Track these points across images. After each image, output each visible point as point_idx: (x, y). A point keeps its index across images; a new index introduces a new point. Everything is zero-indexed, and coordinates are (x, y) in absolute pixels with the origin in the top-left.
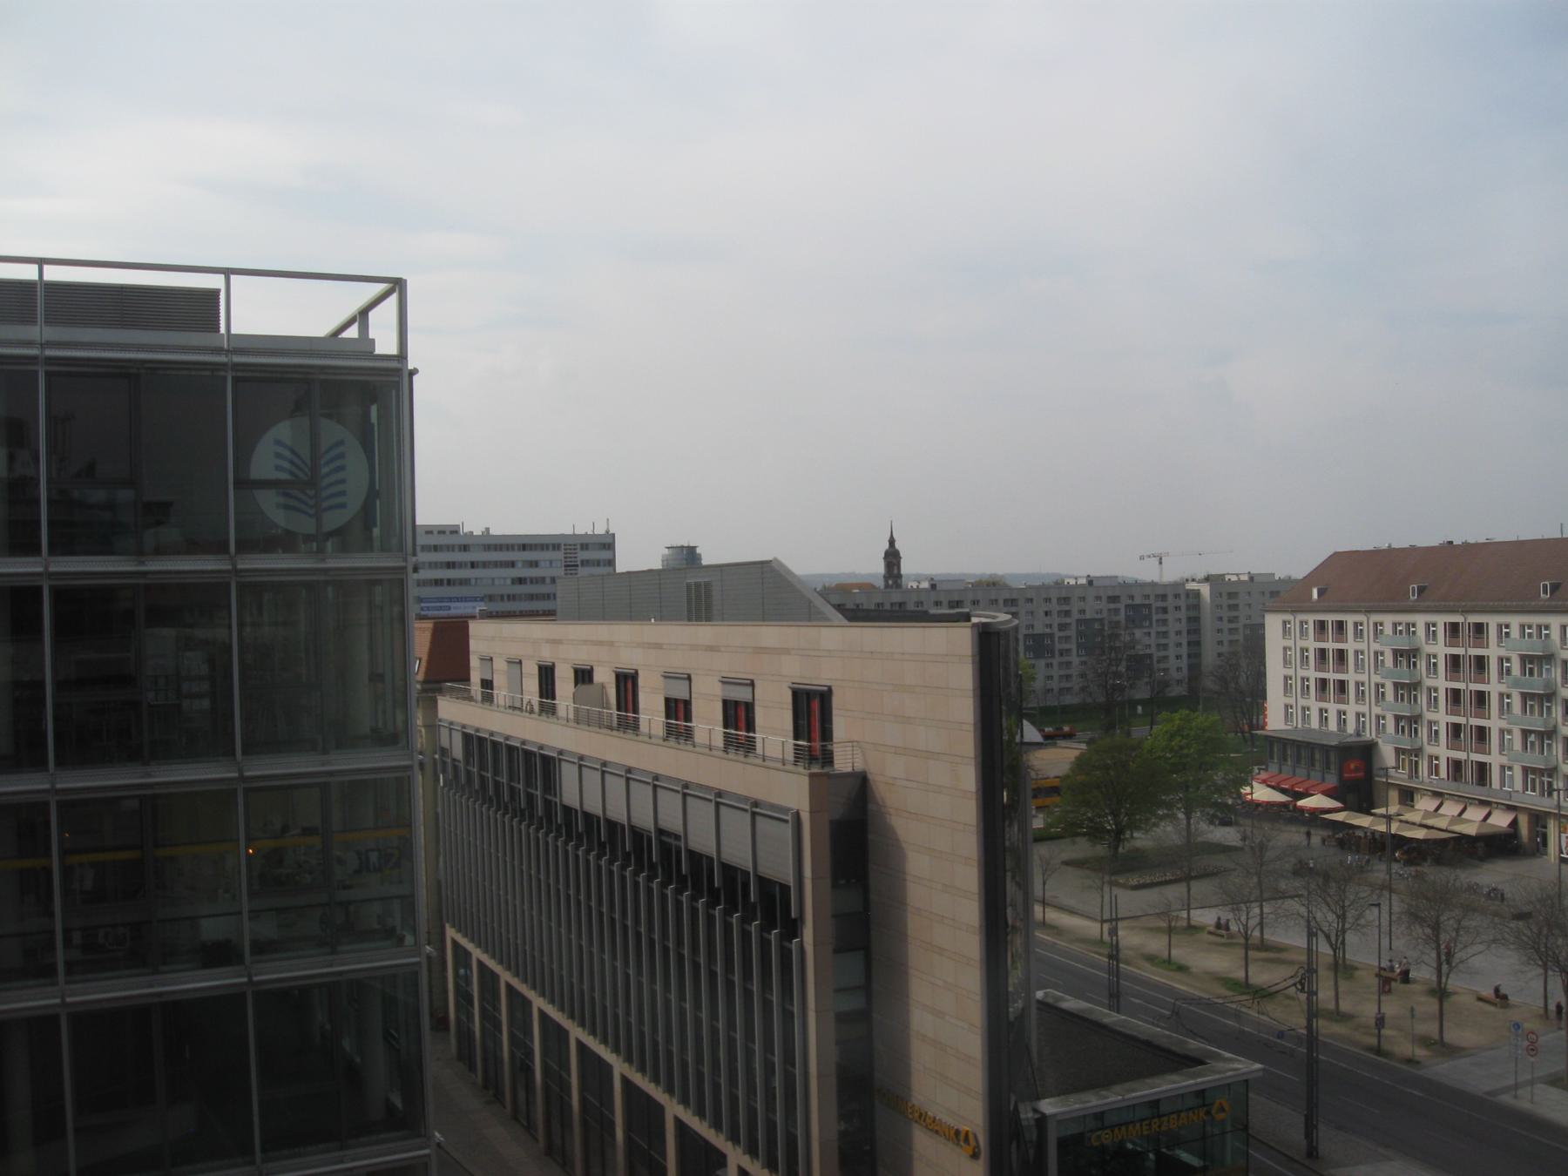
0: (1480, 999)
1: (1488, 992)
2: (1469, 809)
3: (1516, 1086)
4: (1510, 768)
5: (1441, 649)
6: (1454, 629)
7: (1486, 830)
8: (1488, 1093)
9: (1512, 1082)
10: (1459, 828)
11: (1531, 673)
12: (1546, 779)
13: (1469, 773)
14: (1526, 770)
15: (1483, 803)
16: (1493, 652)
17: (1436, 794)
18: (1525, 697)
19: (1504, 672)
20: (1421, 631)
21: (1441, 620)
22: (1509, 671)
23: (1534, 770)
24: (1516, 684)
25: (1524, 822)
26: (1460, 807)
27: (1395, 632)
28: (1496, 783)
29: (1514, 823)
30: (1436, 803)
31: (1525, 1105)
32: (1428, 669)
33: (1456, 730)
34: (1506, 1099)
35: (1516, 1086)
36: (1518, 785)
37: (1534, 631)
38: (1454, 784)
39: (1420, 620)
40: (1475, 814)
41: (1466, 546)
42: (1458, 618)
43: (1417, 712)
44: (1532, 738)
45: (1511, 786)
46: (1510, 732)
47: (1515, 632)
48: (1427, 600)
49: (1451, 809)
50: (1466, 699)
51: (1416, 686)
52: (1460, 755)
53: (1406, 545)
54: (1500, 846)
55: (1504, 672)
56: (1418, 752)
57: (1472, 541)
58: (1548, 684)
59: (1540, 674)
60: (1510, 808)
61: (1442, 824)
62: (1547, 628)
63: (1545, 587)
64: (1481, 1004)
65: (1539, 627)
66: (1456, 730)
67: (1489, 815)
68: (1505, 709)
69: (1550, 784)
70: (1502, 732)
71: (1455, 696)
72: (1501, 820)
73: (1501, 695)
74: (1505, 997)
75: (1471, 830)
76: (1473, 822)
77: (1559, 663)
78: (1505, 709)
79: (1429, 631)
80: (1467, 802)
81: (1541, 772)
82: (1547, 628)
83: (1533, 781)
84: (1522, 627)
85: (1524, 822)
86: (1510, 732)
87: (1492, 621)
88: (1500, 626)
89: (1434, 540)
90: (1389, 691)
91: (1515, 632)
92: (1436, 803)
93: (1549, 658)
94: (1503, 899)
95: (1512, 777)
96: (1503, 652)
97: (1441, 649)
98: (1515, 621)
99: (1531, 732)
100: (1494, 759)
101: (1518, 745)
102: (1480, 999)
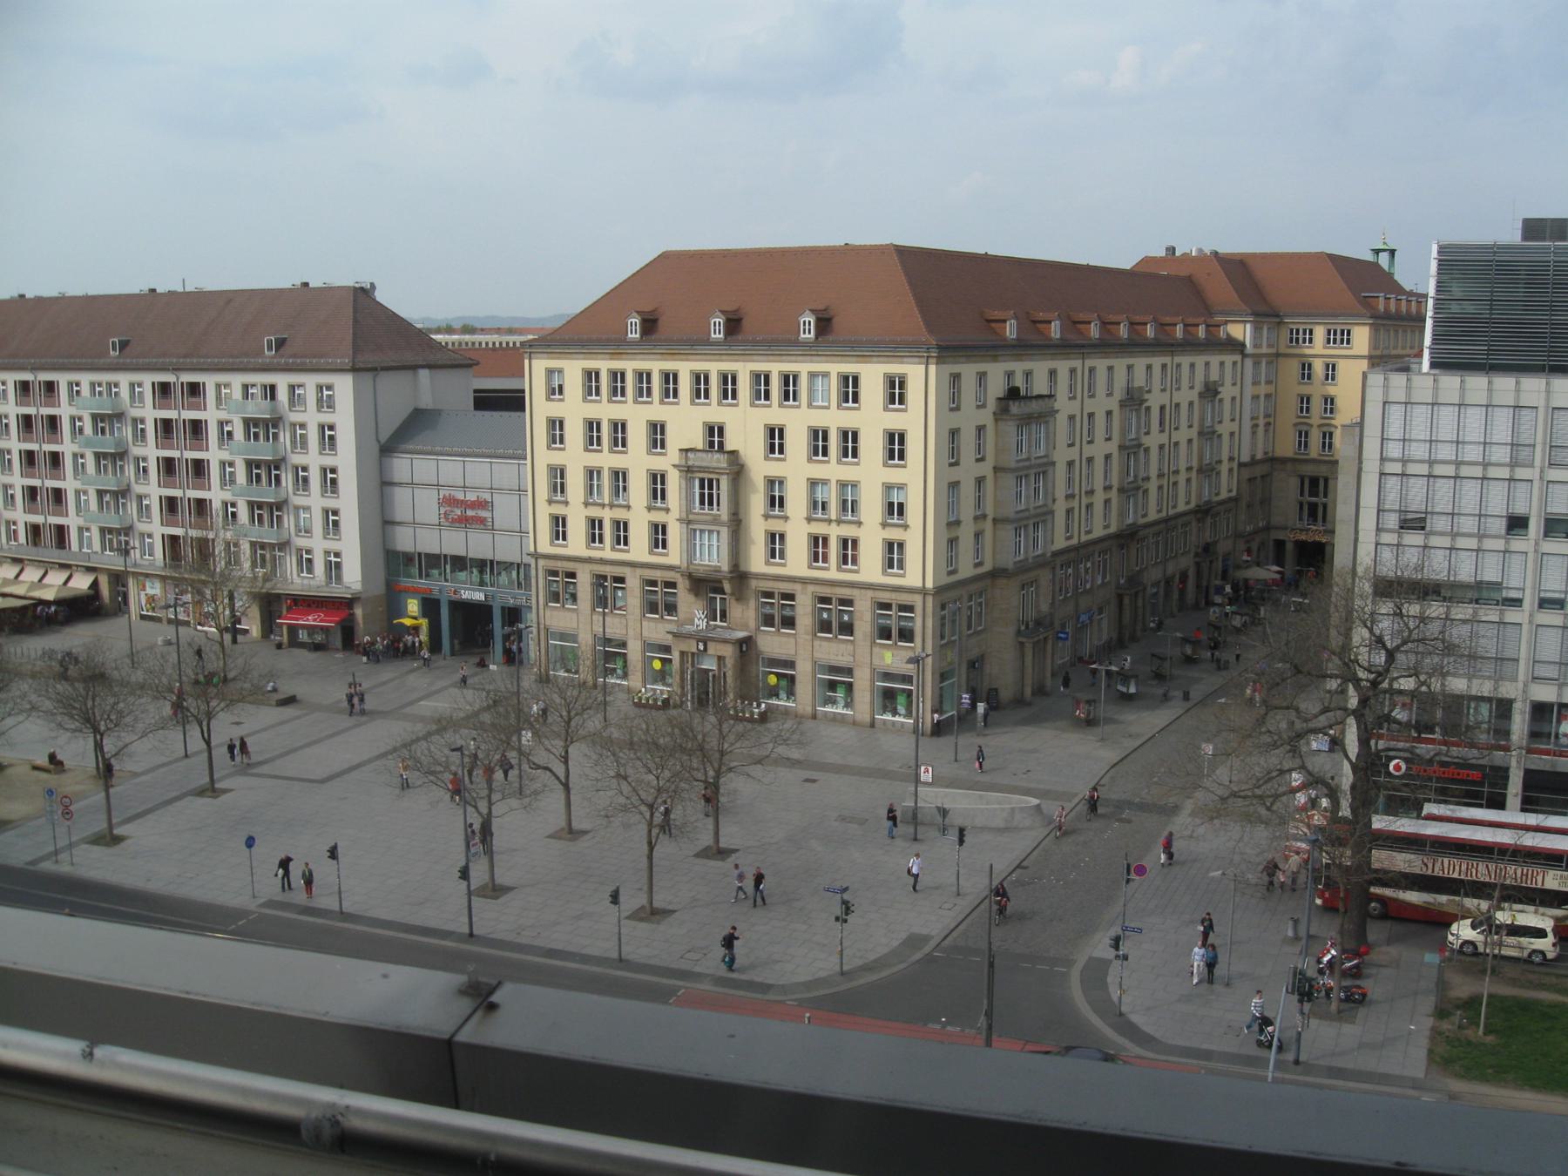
0: (36, 768)
1: (43, 761)
2: (50, 574)
3: (56, 853)
4: (88, 529)
5: (150, 413)
6: (164, 390)
7: (65, 594)
8: (32, 863)
9: (52, 849)
10: (37, 594)
11: (103, 432)
12: (123, 538)
13: (48, 537)
14: (103, 531)
15: (63, 566)
16: (64, 411)
17: (16, 561)
18: (98, 456)
19: (77, 431)
20: (282, 395)
21: (148, 379)
22: (81, 430)
23: (110, 531)
24: (88, 444)
25: (104, 582)
26: (41, 572)
27: (246, 395)
28: (75, 546)
29: (95, 585)
30: (16, 570)
31: (65, 868)
32: (294, 442)
33: (32, 493)
34: (48, 866)
35: (56, 853)
36: (97, 546)
37: (103, 389)
38: (34, 549)
39: (124, 379)
40: (56, 578)
41: (39, 300)
42: (168, 378)
43: (283, 496)
44: (107, 498)
45: (90, 546)
46: (85, 493)
47: (85, 390)
48: (129, 356)
49: (31, 575)
50: (40, 460)
51: (277, 464)
52: (38, 519)
53: (54, 294)
54: (80, 609)
55: (77, 431)
56: (128, 530)
57: (90, 293)
58: (119, 443)
59: (112, 433)
60: (90, 569)
61: (19, 590)
62: (140, 385)
63: (270, 342)
64: (36, 773)
65: (109, 385)
66: (32, 493)
67: (21, 571)
68: (79, 469)
69: (127, 543)
70: (78, 492)
71: (168, 466)
72: (81, 583)
73: (75, 455)
74: (61, 763)
75: (49, 595)
76: (53, 586)
77: (129, 422)
78: (79, 469)
79: (135, 392)
80: (47, 567)
81: (119, 532)
82: (116, 385)
83: (111, 541)
84: (93, 385)
85: (104, 582)
86: (85, 493)
87: (62, 379)
88: (70, 384)
89: (284, 279)
90: (90, 461)
91: (85, 390)
92: (16, 570)
93: (119, 416)
94: (76, 659)
95: (90, 538)
96: (74, 412)
97: (150, 413)
98: (85, 379)
99: (106, 492)
100: (72, 521)
101: (94, 505)
102: (36, 768)
